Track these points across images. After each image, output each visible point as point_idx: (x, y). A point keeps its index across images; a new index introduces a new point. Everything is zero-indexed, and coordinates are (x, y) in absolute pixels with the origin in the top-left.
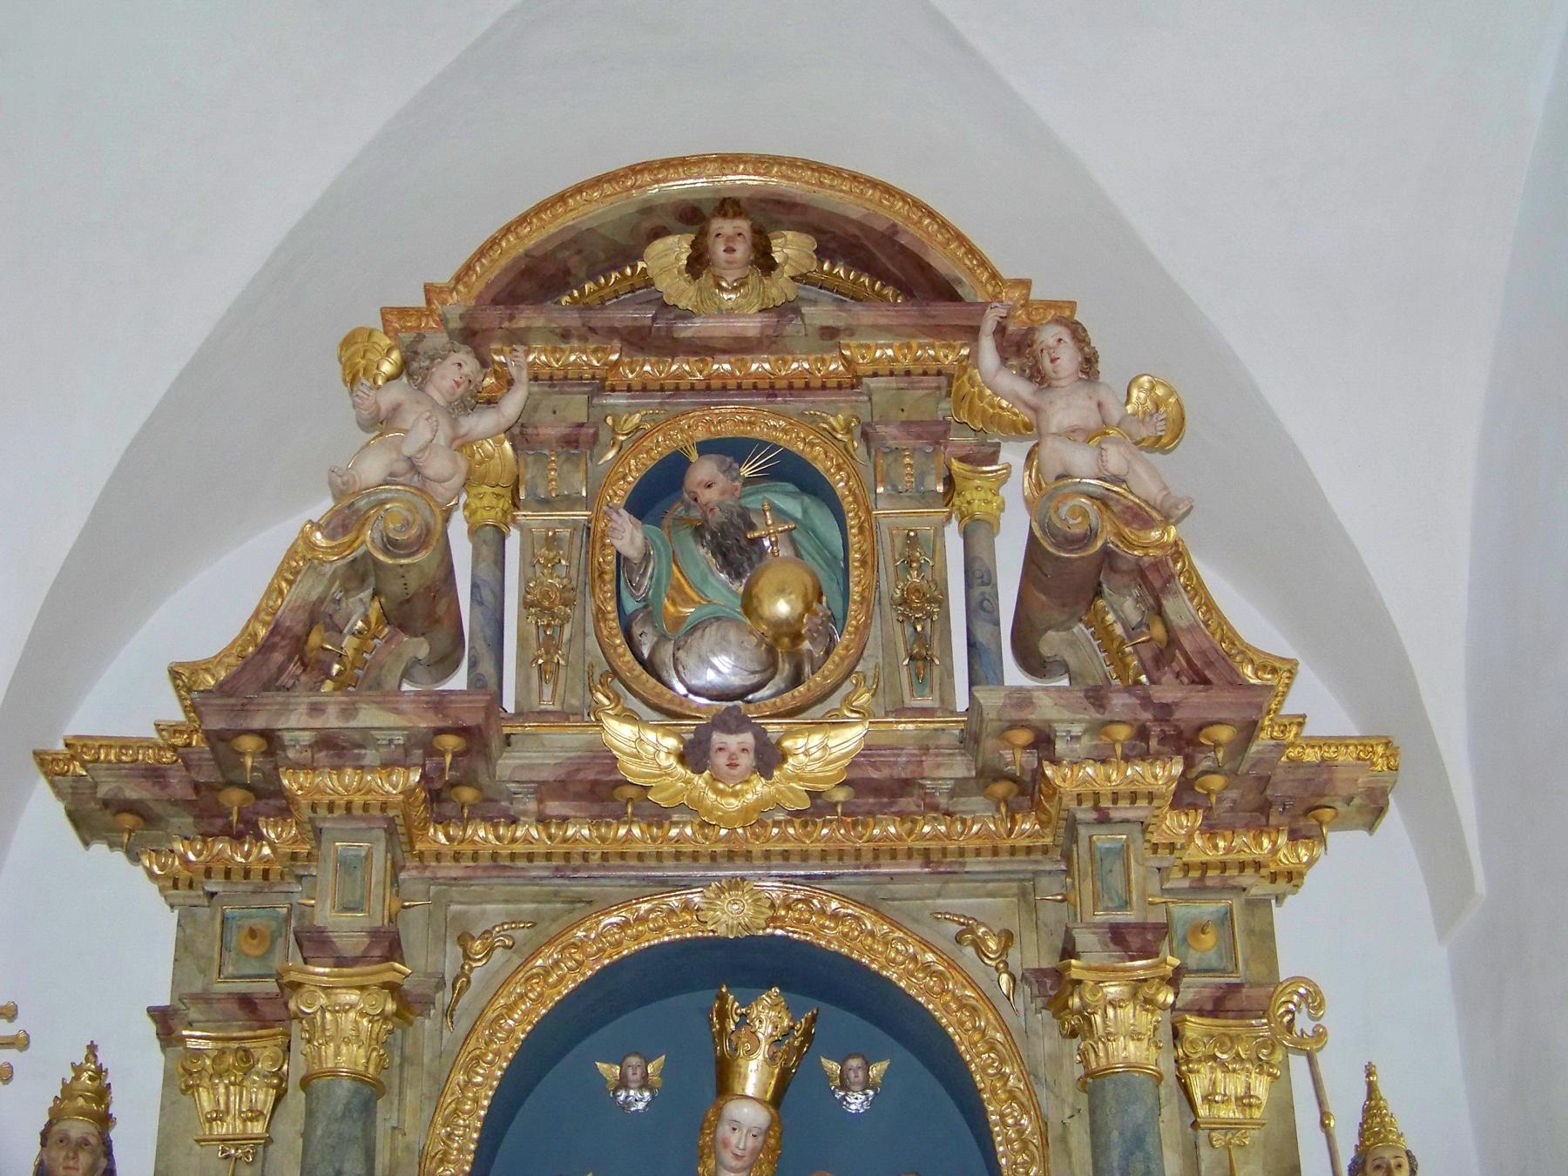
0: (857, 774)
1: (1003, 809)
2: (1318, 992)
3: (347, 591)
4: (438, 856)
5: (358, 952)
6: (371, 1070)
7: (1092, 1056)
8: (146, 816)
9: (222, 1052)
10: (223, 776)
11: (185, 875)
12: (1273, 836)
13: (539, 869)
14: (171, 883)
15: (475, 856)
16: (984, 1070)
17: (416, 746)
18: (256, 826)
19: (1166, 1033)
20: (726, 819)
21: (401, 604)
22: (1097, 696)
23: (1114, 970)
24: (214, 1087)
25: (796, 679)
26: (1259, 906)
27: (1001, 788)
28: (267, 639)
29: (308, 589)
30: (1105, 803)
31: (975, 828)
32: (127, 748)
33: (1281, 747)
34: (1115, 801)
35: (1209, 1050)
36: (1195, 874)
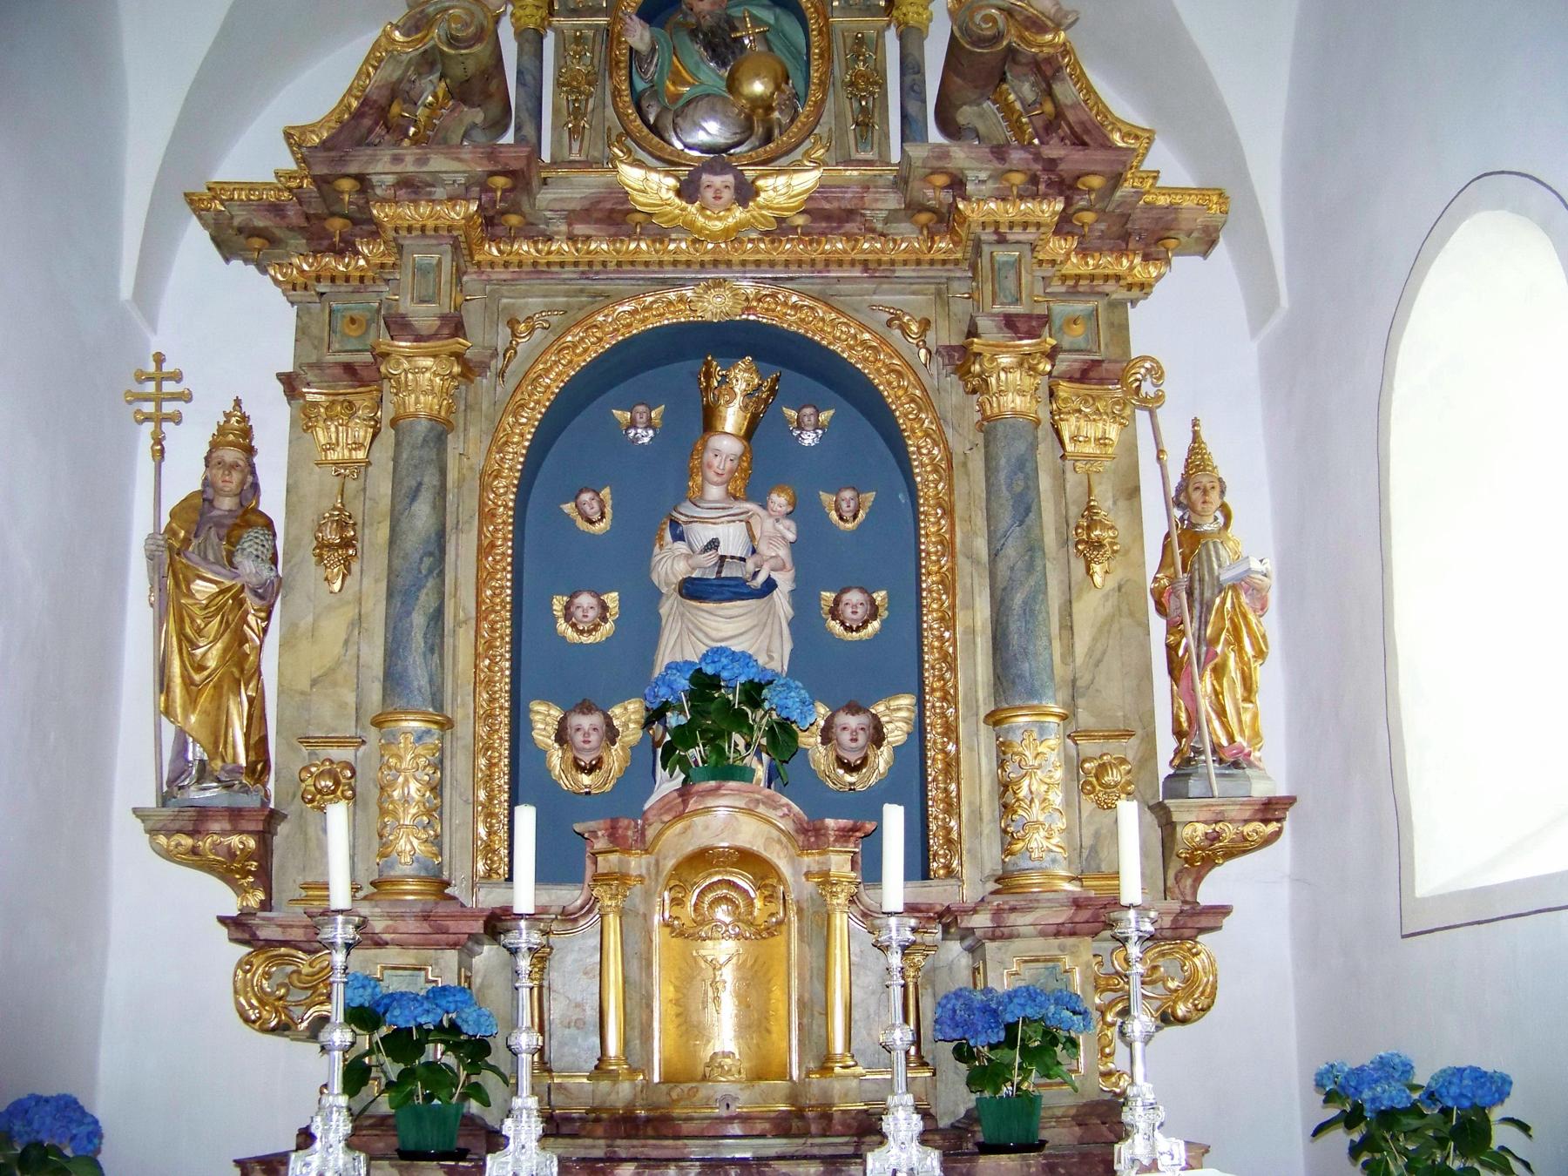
0: (812, 205)
1: (925, 232)
2: (1160, 367)
3: (420, 75)
4: (492, 264)
5: (432, 331)
6: (443, 413)
7: (988, 407)
8: (272, 241)
9: (333, 402)
10: (328, 208)
11: (301, 280)
12: (1131, 257)
13: (568, 273)
14: (291, 288)
15: (520, 264)
16: (906, 415)
17: (474, 184)
18: (354, 245)
19: (1043, 393)
20: (713, 237)
21: (461, 83)
22: (1000, 152)
23: (1007, 346)
24: (328, 428)
25: (768, 138)
26: (1118, 306)
27: (924, 217)
28: (358, 109)
29: (390, 73)
30: (1003, 230)
31: (904, 246)
32: (255, 190)
33: (1140, 194)
34: (1011, 228)
35: (1075, 405)
36: (1071, 283)
